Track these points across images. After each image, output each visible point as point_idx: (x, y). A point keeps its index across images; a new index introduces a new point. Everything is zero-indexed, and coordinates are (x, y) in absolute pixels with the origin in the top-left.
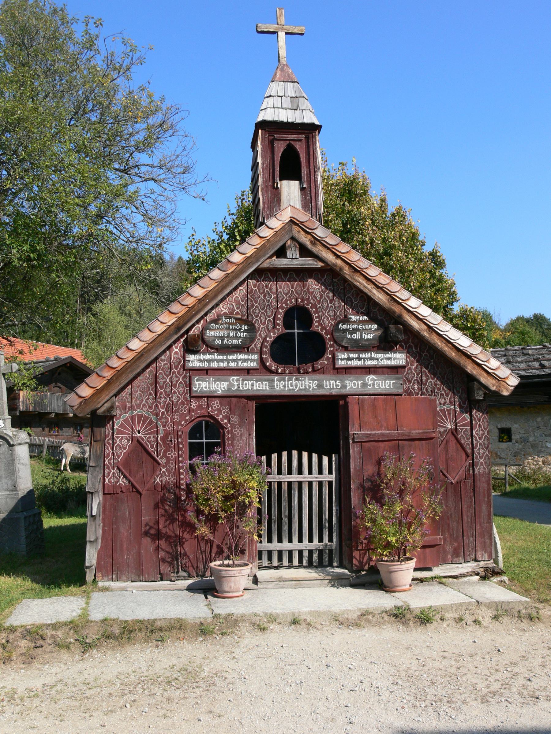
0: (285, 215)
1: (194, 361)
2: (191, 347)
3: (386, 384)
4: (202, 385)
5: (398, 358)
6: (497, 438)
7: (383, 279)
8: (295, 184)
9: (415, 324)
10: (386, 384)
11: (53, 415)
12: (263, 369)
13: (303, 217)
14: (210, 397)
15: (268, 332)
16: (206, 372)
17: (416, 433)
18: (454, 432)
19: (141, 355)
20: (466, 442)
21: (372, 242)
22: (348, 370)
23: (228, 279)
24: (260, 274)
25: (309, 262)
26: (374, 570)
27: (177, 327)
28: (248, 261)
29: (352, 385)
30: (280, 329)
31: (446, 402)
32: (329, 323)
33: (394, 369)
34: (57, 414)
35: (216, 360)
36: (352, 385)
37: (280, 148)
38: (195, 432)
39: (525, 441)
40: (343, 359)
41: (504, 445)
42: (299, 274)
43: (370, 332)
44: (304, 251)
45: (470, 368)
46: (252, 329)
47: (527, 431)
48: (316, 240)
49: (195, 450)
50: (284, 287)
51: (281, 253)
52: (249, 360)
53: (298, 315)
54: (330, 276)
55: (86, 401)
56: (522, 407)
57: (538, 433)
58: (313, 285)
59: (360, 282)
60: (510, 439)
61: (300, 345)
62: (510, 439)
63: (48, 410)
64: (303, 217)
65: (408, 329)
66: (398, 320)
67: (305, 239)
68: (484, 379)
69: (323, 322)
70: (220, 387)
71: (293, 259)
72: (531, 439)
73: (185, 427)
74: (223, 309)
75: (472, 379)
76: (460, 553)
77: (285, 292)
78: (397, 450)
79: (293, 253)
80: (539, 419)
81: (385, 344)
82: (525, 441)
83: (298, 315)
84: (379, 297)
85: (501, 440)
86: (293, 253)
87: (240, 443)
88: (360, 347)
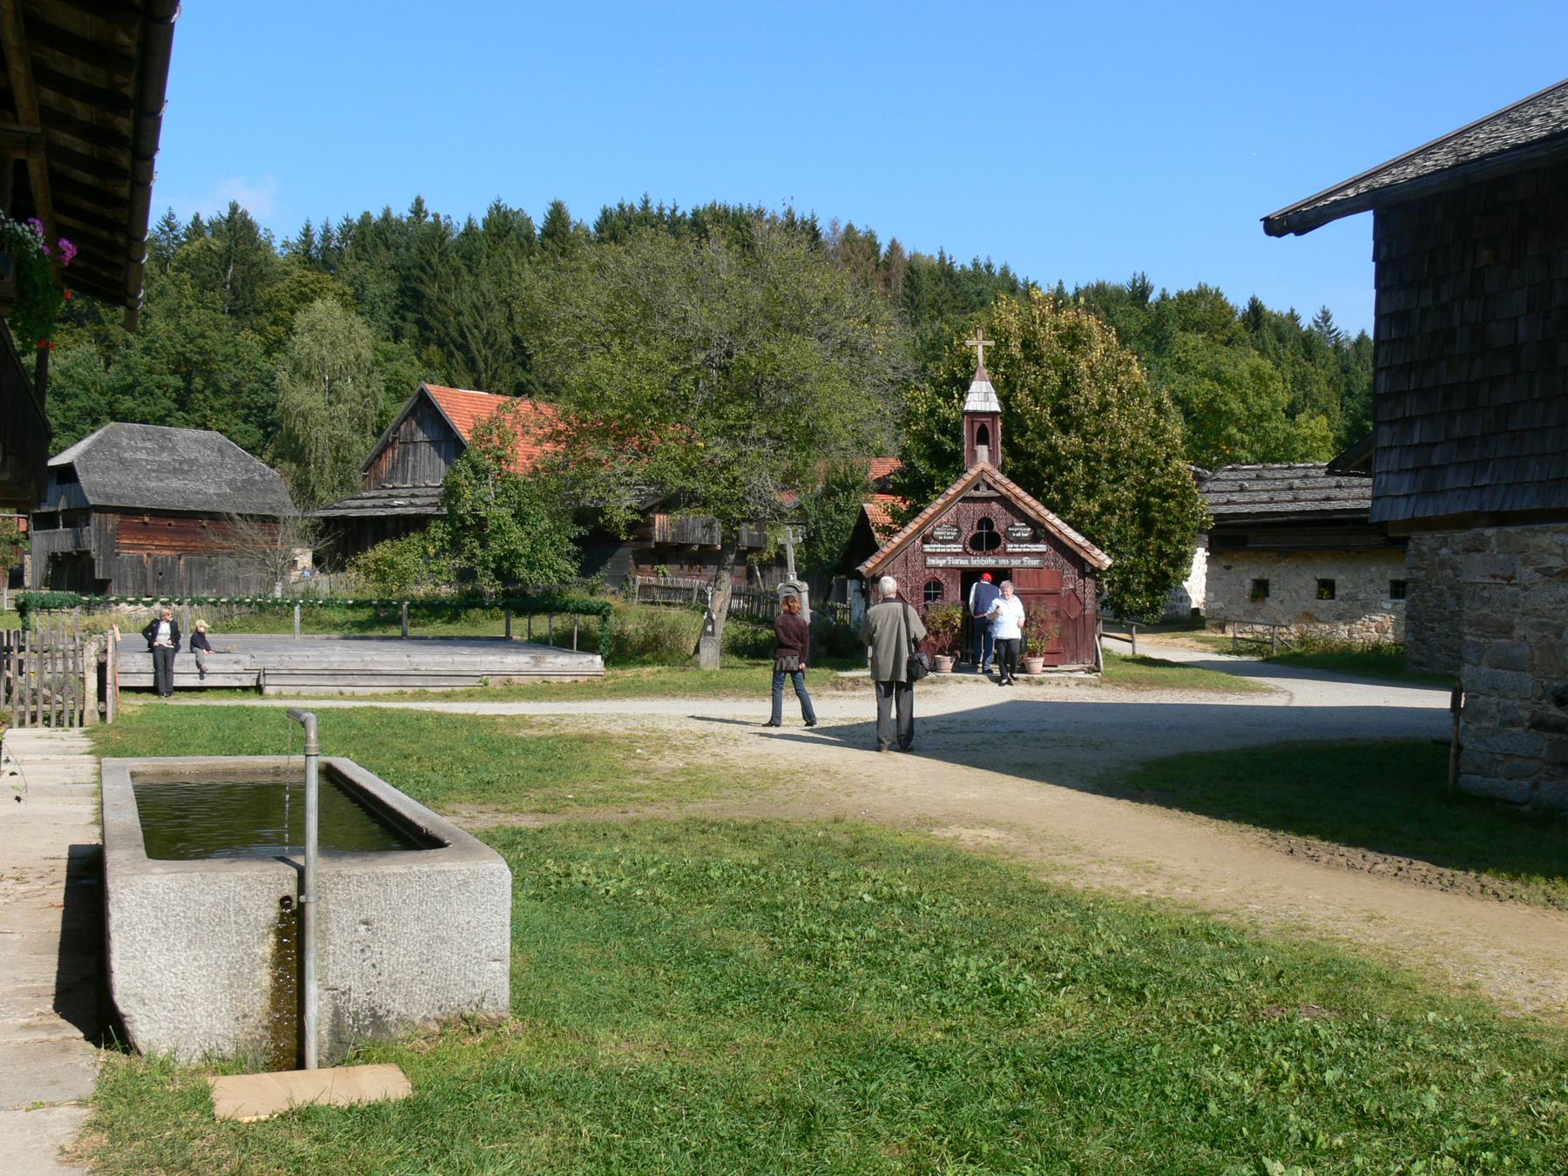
0: (979, 467)
1: (927, 548)
2: (926, 540)
3: (1035, 562)
4: (931, 561)
5: (1042, 547)
6: (1314, 594)
7: (1034, 503)
8: (985, 447)
9: (1052, 529)
10: (1035, 562)
11: (696, 548)
12: (965, 553)
13: (989, 467)
14: (936, 568)
15: (969, 532)
16: (934, 554)
17: (1050, 590)
18: (1074, 590)
19: (899, 546)
20: (1081, 596)
21: (1087, 401)
22: (1013, 554)
23: (947, 504)
24: (965, 500)
25: (991, 493)
26: (1023, 665)
27: (919, 530)
28: (958, 493)
29: (1015, 562)
30: (975, 531)
31: (1070, 573)
32: (1003, 527)
33: (1040, 553)
34: (701, 546)
35: (939, 548)
36: (1015, 562)
37: (977, 426)
38: (927, 587)
39: (1353, 598)
40: (1010, 548)
41: (1324, 604)
42: (988, 500)
43: (1026, 532)
44: (989, 487)
45: (1083, 555)
46: (960, 531)
47: (1356, 586)
48: (995, 482)
49: (927, 597)
50: (978, 506)
51: (977, 488)
52: (958, 548)
53: (986, 522)
54: (1004, 501)
55: (870, 570)
56: (1347, 551)
57: (1370, 588)
58: (995, 505)
59: (1021, 505)
60: (1332, 596)
61: (986, 539)
62: (1332, 596)
63: (691, 540)
64: (989, 467)
65: (1047, 531)
66: (1042, 526)
67: (990, 480)
68: (1091, 561)
69: (999, 527)
70: (941, 562)
71: (983, 492)
72: (1361, 596)
73: (922, 584)
74: (944, 519)
75: (1085, 560)
76: (1075, 658)
77: (978, 510)
78: (1039, 599)
79: (983, 488)
80: (1373, 569)
81: (1035, 539)
82: (1353, 598)
83: (986, 522)
84: (1032, 513)
85: (1320, 596)
86: (983, 488)
87: (952, 593)
88: (1020, 541)
